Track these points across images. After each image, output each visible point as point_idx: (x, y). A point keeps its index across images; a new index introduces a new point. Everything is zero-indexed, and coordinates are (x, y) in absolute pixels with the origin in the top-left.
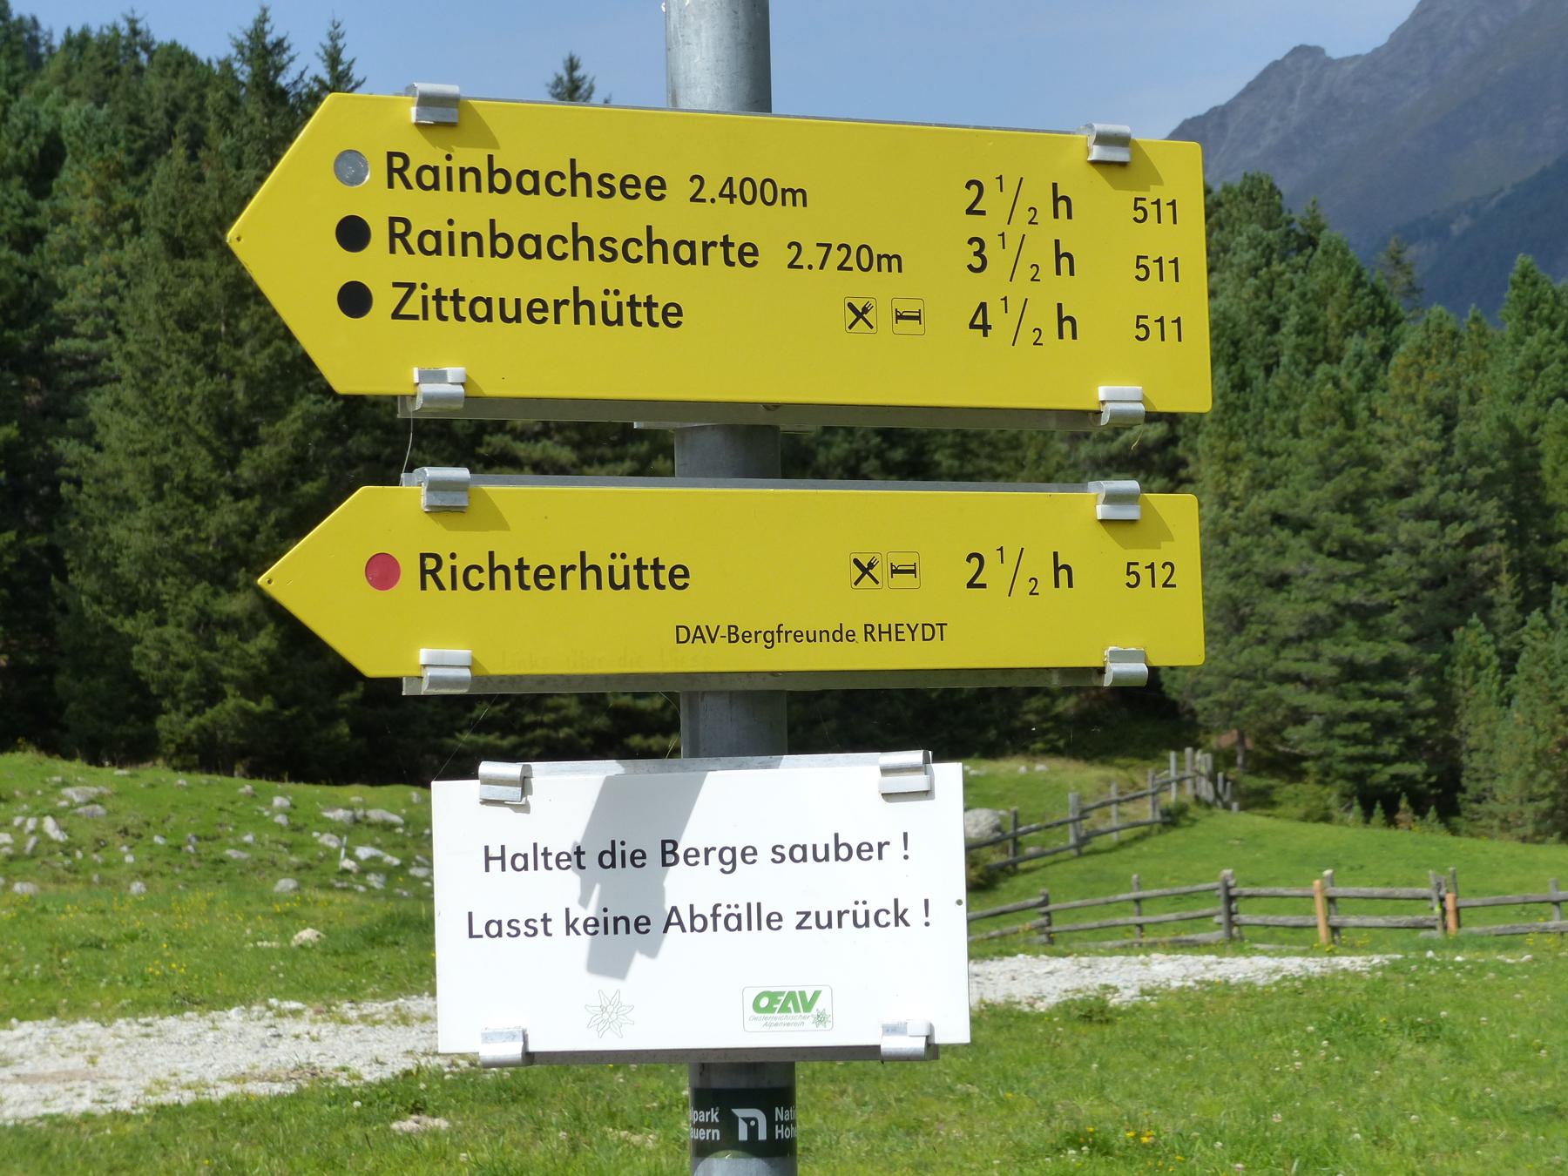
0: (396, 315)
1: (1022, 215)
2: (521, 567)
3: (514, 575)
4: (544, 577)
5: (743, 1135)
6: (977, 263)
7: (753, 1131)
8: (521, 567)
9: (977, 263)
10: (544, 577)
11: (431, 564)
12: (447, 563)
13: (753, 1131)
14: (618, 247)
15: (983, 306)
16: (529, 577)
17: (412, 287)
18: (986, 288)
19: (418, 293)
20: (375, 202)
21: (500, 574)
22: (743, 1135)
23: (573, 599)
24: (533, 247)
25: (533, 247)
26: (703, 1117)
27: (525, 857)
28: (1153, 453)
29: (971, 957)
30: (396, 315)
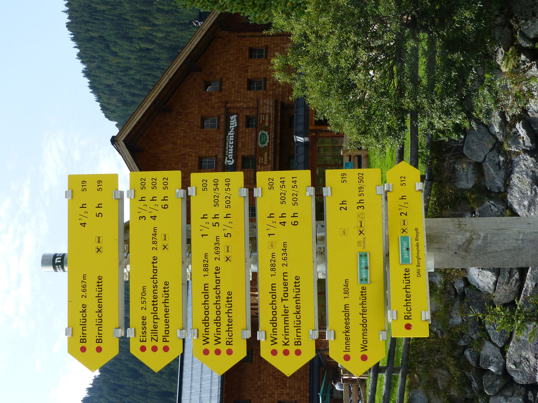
0: (157, 341)
1: (145, 208)
2: (406, 300)
3: (408, 302)
4: (408, 296)
5: (60, 261)
6: (144, 218)
7: (59, 260)
8: (406, 300)
9: (144, 218)
10: (408, 296)
11: (406, 317)
12: (406, 314)
13: (59, 260)
14: (217, 295)
15: (151, 217)
16: (408, 299)
17: (152, 338)
18: (148, 216)
19: (153, 337)
20: (280, 348)
21: (408, 304)
22: (60, 261)
23: (413, 290)
24: (218, 312)
25: (218, 312)
26: (58, 269)
27: (272, 295)
28: (318, 182)
29: (316, 220)
30: (157, 341)
